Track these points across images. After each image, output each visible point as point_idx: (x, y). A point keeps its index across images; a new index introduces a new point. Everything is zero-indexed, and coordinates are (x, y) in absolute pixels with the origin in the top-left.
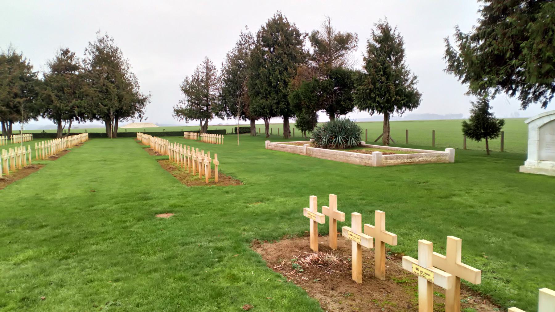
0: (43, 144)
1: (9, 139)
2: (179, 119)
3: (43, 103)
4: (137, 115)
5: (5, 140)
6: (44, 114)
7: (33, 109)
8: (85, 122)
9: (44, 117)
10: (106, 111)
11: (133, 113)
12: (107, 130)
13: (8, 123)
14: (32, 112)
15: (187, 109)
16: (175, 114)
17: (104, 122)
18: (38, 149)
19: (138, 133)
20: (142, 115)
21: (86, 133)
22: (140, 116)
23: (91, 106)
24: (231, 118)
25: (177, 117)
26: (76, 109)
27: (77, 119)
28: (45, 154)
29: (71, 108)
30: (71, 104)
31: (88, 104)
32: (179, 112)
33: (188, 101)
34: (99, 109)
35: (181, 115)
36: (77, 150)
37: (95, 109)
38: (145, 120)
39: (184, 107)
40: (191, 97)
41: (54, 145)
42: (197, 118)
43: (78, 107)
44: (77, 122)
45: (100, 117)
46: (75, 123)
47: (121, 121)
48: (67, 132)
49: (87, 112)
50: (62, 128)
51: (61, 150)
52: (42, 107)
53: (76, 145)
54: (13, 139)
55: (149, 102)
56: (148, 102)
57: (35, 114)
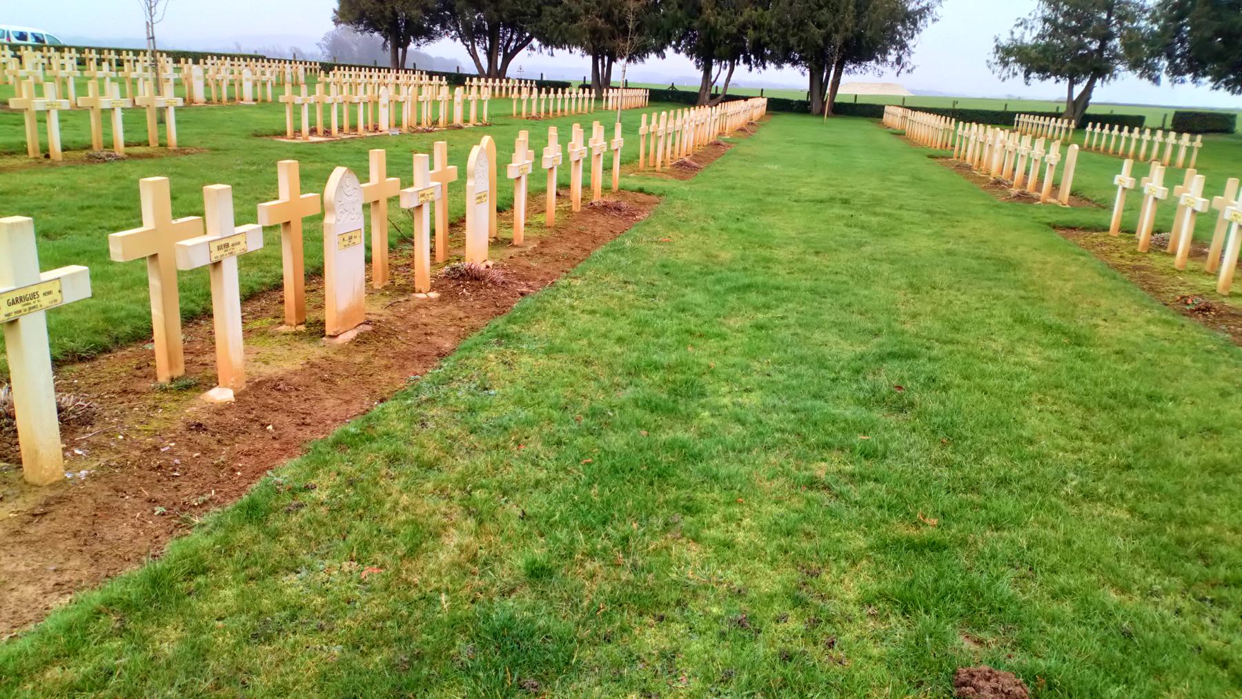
0: (665, 121)
1: (599, 98)
2: (1005, 74)
3: (679, 14)
4: (892, 56)
5: (590, 99)
6: (678, 44)
7: (658, 30)
8: (764, 68)
9: (678, 51)
10: (820, 42)
11: (884, 52)
12: (811, 93)
13: (606, 58)
14: (655, 36)
15: (1035, 46)
16: (997, 60)
17: (807, 72)
18: (648, 136)
19: (887, 108)
20: (905, 59)
21: (762, 96)
22: (899, 60)
23: (786, 26)
24: (1183, 82)
25: (999, 68)
26: (750, 32)
27: (747, 61)
28: (665, 155)
29: (738, 30)
30: (741, 19)
31: (779, 21)
32: (1012, 54)
33: (1045, 20)
34: (804, 35)
35: (1015, 61)
36: (746, 147)
37: (793, 35)
38: (908, 71)
39: (1029, 38)
40: (1056, 9)
41: (693, 124)
42: (1058, 72)
43: (755, 28)
44: (747, 66)
45: (801, 58)
46: (741, 69)
47: (849, 71)
48: (720, 92)
49: (772, 40)
50: (713, 80)
51: (706, 143)
52: (676, 23)
53: (742, 130)
54: (607, 98)
55: (934, 20)
56: (929, 19)
57: (659, 42)
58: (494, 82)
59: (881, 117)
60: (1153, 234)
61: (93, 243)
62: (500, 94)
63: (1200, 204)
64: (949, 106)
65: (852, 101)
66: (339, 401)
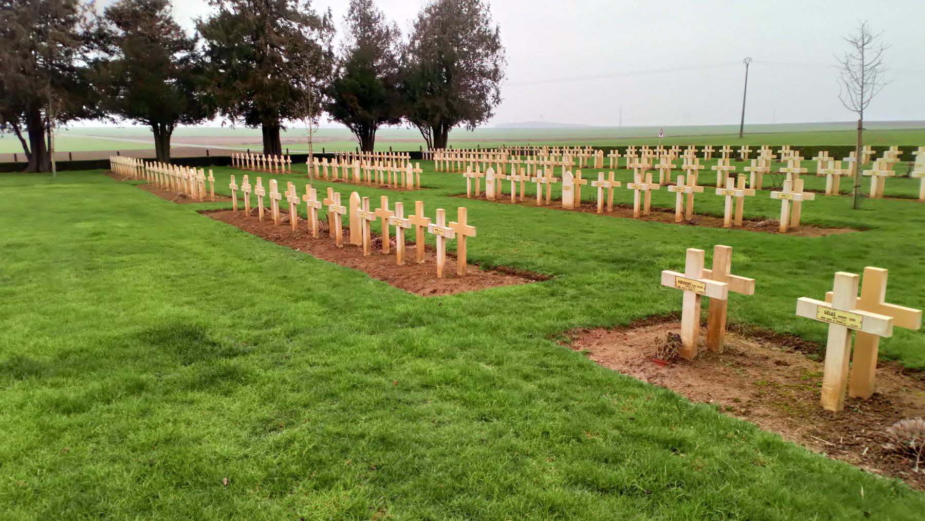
5: (286, 164)
56: (411, 36)
58: (273, 157)
59: (110, 168)
60: (372, 238)
61: (417, 431)
62: (274, 169)
63: (318, 204)
64: (52, 148)
65: (13, 161)
66: (859, 75)
